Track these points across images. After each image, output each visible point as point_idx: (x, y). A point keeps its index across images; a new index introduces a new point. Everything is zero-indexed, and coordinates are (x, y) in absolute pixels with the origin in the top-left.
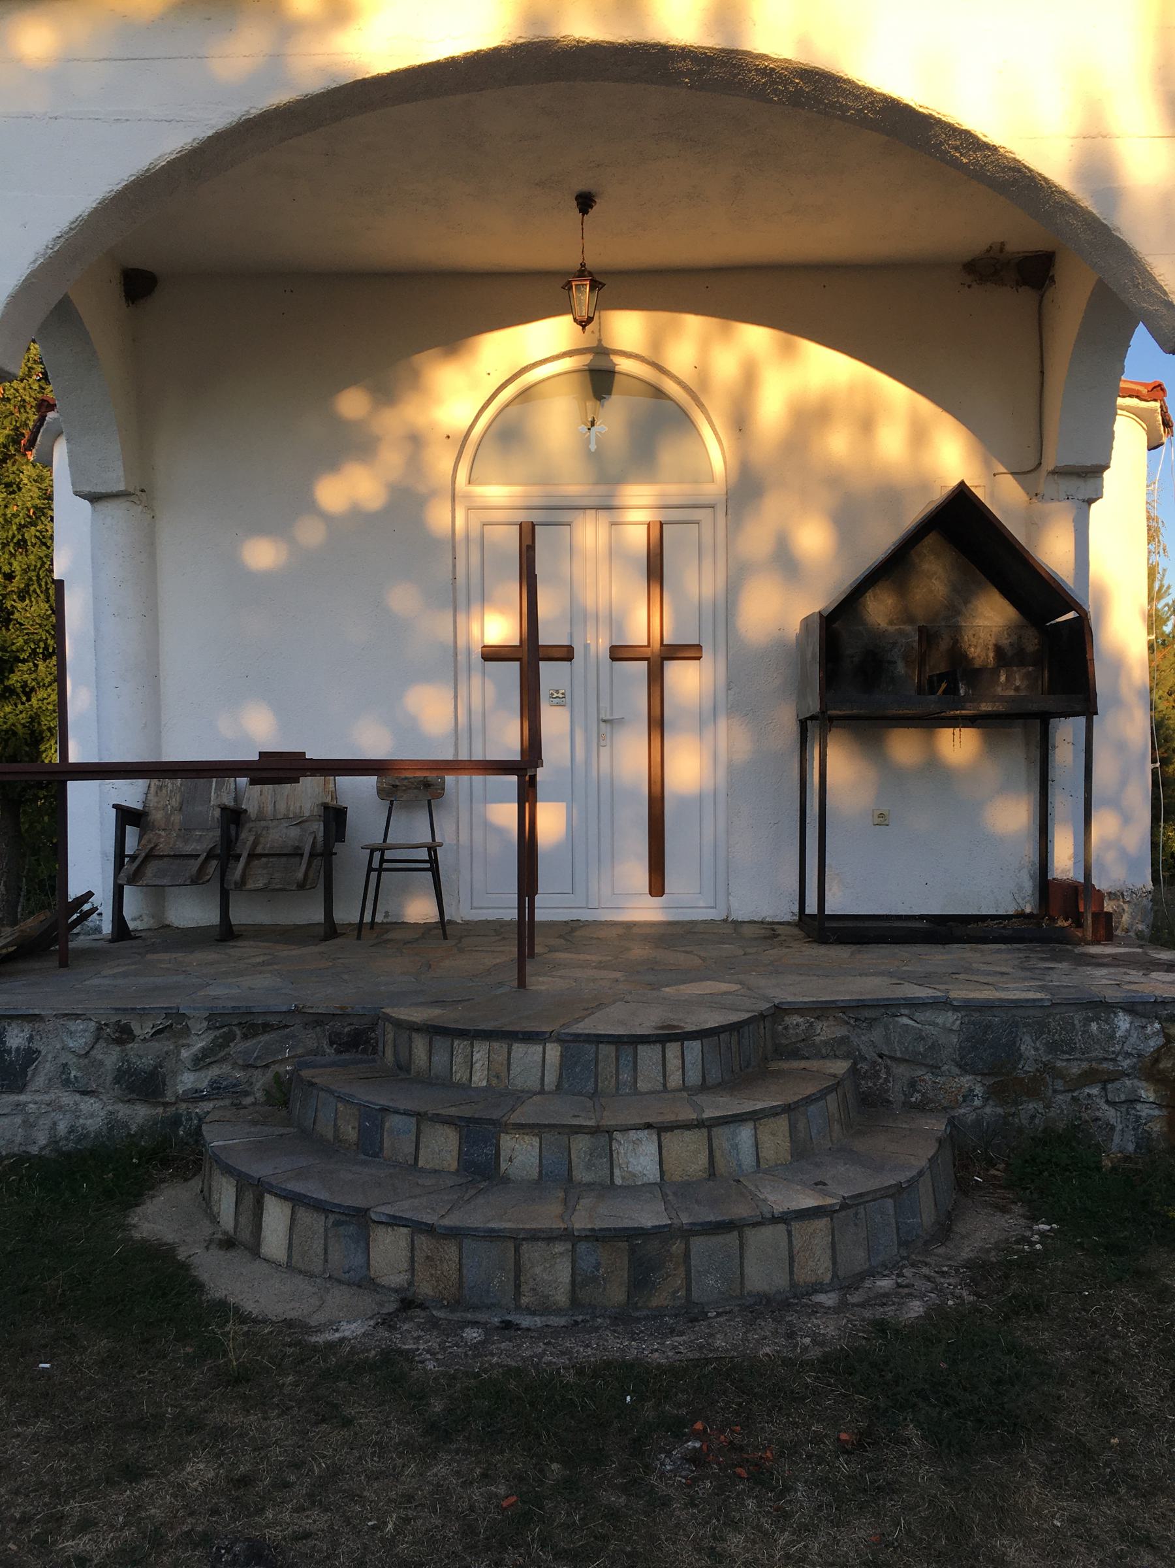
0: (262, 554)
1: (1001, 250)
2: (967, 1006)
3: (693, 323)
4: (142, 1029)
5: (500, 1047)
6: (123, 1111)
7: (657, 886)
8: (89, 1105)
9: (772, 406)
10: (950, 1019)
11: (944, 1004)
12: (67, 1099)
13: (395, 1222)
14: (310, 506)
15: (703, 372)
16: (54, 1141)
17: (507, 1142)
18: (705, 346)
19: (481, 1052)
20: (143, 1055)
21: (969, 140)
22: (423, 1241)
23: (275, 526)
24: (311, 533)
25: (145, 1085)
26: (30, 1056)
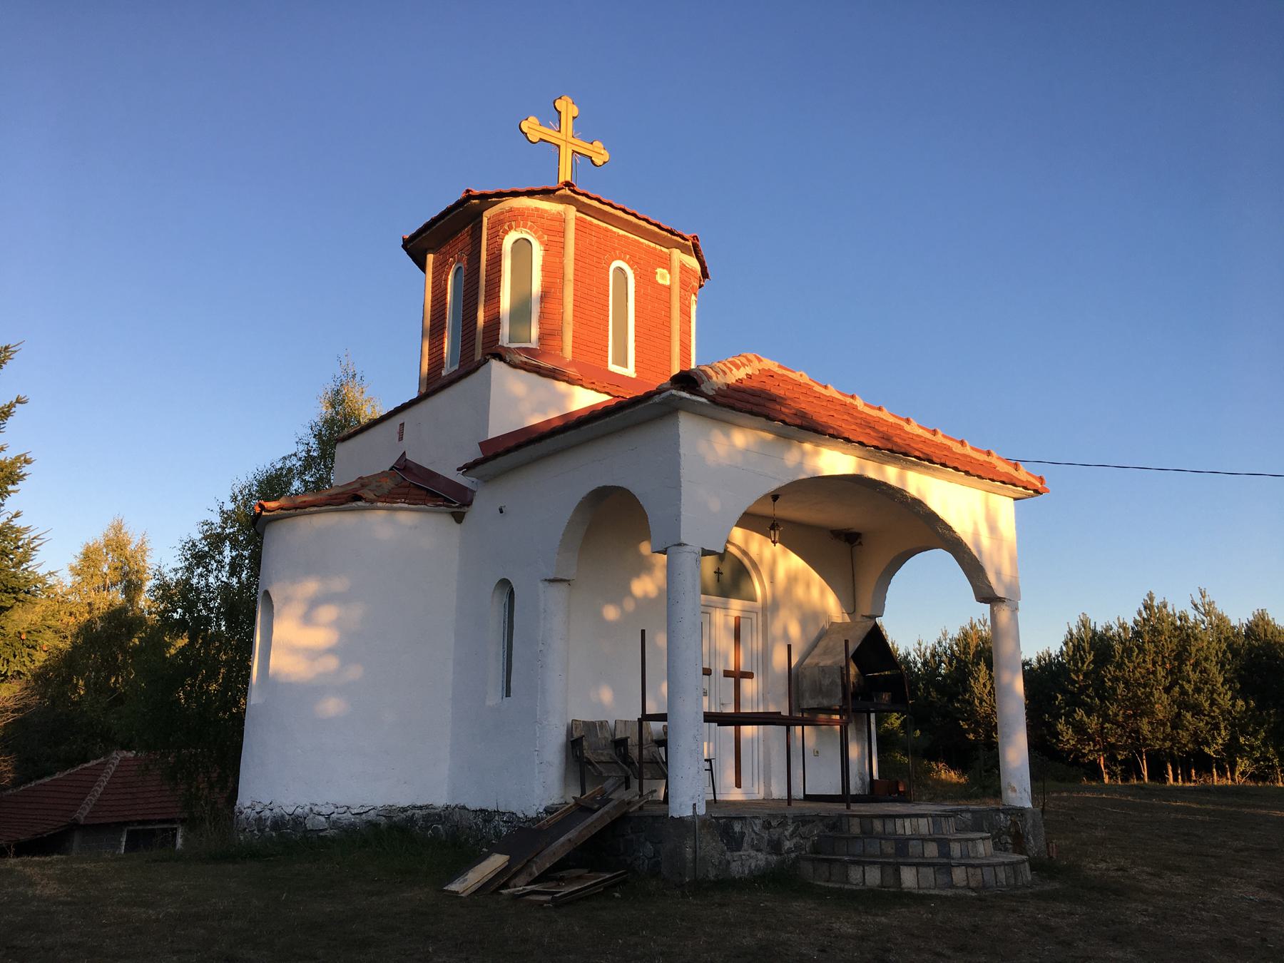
0: (611, 613)
1: (1236, 653)
2: (973, 812)
3: (757, 536)
4: (774, 823)
5: (914, 820)
6: (770, 858)
7: (738, 785)
8: (760, 855)
9: (781, 574)
10: (969, 816)
11: (968, 811)
12: (753, 853)
13: (959, 865)
14: (628, 592)
15: (760, 555)
16: (751, 872)
17: (952, 845)
18: (761, 545)
19: (907, 822)
20: (775, 833)
21: (949, 528)
22: (970, 870)
23: (617, 601)
24: (629, 605)
25: (775, 847)
26: (742, 834)
